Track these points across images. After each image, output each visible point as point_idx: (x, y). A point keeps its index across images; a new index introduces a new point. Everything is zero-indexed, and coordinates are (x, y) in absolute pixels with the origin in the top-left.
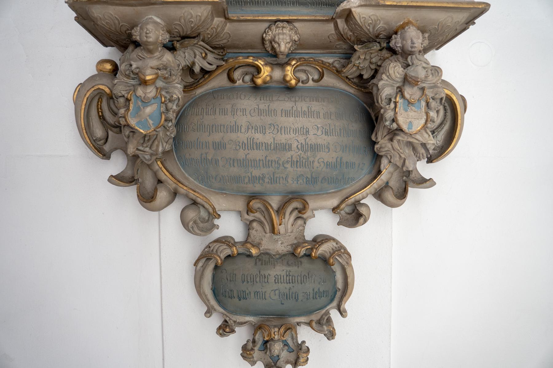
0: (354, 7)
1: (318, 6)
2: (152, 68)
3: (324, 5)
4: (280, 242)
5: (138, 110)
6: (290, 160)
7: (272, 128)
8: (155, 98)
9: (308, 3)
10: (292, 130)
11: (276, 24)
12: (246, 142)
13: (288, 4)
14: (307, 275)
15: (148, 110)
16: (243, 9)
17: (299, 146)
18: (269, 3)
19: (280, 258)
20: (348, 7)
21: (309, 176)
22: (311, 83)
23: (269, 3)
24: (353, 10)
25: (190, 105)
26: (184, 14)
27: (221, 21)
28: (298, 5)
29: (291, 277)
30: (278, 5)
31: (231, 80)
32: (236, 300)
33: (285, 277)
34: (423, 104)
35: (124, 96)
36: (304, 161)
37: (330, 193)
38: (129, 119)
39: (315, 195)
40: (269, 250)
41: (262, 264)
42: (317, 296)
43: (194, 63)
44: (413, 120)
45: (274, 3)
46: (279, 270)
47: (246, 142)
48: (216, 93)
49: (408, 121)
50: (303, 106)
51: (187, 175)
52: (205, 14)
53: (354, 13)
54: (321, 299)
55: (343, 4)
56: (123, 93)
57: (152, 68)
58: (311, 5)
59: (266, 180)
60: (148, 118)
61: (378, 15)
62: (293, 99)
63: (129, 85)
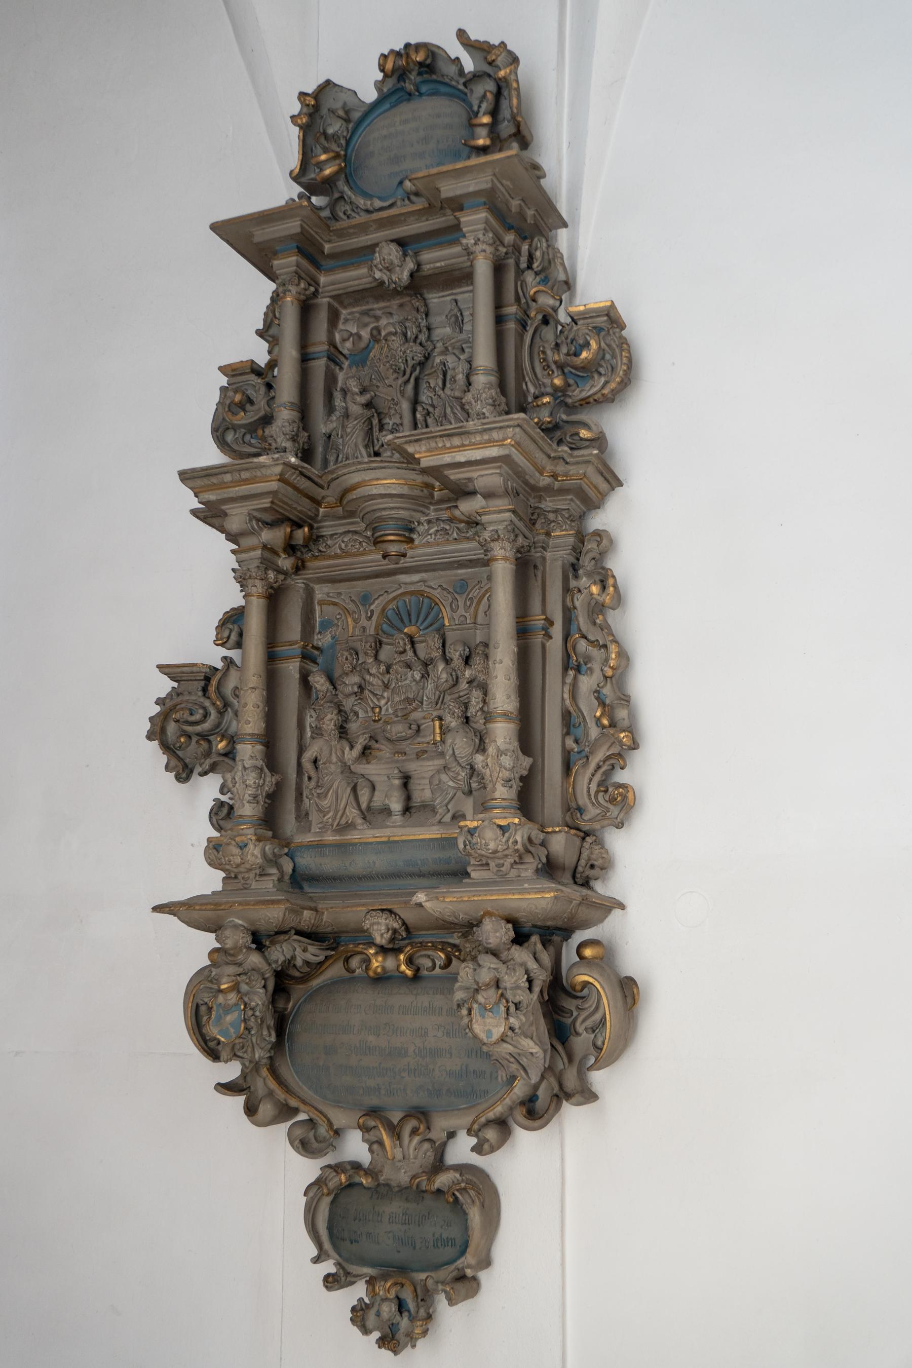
2: (228, 976)
4: (403, 1171)
5: (219, 1018)
6: (406, 1067)
7: (388, 1028)
8: (237, 1005)
10: (408, 1032)
12: (358, 1045)
14: (427, 1214)
15: (229, 1018)
17: (417, 1051)
19: (400, 1191)
21: (431, 1088)
22: (437, 970)
25: (305, 1001)
29: (407, 1217)
31: (349, 970)
32: (348, 1243)
33: (401, 1215)
34: (502, 1008)
35: (206, 1003)
36: (423, 1069)
37: (460, 1109)
38: (211, 1028)
39: (442, 1111)
40: (391, 1180)
41: (378, 1198)
42: (439, 1244)
43: (294, 957)
44: (491, 1028)
46: (395, 1207)
47: (358, 1045)
48: (336, 983)
49: (486, 1028)
50: (424, 1000)
51: (300, 1084)
52: (281, 915)
54: (446, 1248)
56: (206, 1000)
57: (228, 976)
59: (383, 1092)
60: (229, 1026)
62: (415, 992)
63: (213, 991)
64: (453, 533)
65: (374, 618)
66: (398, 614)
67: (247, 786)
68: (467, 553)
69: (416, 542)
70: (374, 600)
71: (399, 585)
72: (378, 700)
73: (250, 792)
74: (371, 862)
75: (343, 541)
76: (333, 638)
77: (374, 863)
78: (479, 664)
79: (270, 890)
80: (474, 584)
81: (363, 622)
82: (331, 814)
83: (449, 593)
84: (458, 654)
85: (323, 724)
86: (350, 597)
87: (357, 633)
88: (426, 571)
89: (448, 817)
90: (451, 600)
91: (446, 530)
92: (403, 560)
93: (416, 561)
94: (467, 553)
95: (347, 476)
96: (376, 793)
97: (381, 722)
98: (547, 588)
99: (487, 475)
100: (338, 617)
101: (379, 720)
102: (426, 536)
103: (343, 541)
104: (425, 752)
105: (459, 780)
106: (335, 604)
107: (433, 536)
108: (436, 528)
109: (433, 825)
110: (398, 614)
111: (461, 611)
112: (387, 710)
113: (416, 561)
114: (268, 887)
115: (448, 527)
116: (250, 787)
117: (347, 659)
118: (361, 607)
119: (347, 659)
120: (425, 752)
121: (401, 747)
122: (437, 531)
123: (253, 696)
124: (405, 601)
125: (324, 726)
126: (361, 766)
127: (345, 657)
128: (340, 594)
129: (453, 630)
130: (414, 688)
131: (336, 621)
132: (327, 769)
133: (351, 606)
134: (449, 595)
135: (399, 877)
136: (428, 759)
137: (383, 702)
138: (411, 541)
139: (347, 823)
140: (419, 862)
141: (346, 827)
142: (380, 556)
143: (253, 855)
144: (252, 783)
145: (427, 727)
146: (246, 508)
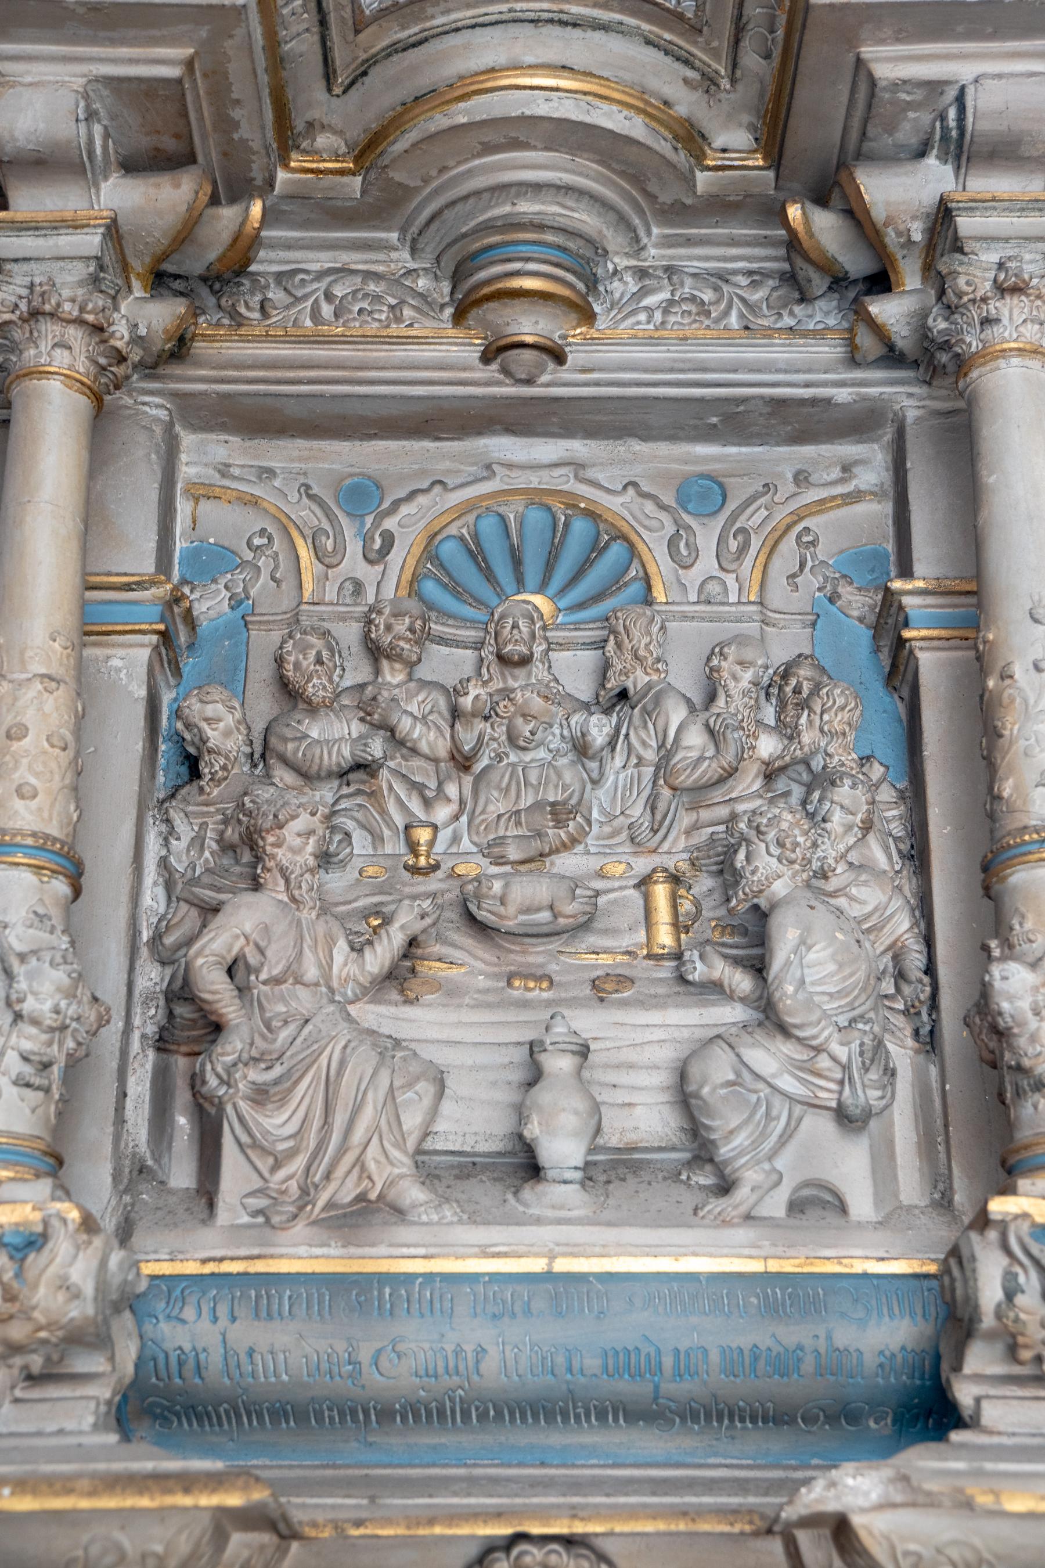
0: (863, 1510)
1: (715, 1424)
3: (742, 1420)
9: (668, 1414)
11: (515, 1552)
13: (577, 1417)
16: (371, 1439)
18: (492, 1413)
20: (832, 1506)
23: (492, 1413)
24: (857, 1520)
26: (86, 1549)
27: (262, 1548)
28: (621, 1421)
30: (530, 1420)
45: (512, 1414)
53: (863, 1535)
55: (809, 1491)
58: (683, 1419)
61: (977, 1542)
64: (726, 313)
65: (396, 557)
66: (477, 554)
67: (18, 1017)
68: (780, 377)
69: (601, 323)
70: (397, 504)
71: (488, 467)
72: (427, 803)
73: (27, 1045)
74: (469, 1348)
75: (329, 297)
76: (236, 603)
77: (481, 1351)
78: (842, 708)
79: (85, 1440)
80: (750, 491)
81: (353, 564)
82: (299, 1163)
83: (663, 507)
84: (748, 675)
85: (278, 845)
86: (308, 487)
87: (331, 595)
88: (591, 432)
89: (776, 1205)
90: (670, 529)
91: (703, 302)
92: (550, 372)
93: (597, 384)
94: (780, 377)
95: (466, 34)
96: (447, 1107)
97: (440, 874)
98: (133, 842)
99: (1012, 75)
100: (257, 541)
101: (436, 867)
102: (633, 312)
103: (329, 297)
104: (624, 981)
105: (819, 1075)
106: (253, 502)
107: (658, 316)
108: (665, 295)
109: (726, 1223)
110: (477, 554)
111: (707, 564)
112: (456, 839)
113: (597, 384)
114: (70, 1425)
115: (707, 296)
116: (35, 1022)
117: (319, 661)
118: (344, 520)
119: (319, 661)
120: (624, 981)
121: (531, 959)
122: (671, 302)
123: (50, 703)
124: (503, 519)
125: (280, 852)
126: (382, 1009)
127: (312, 655)
128: (271, 472)
129: (685, 617)
130: (568, 776)
131: (249, 555)
132: (282, 999)
133: (306, 514)
134: (664, 516)
135: (550, 1418)
136: (642, 1003)
137: (442, 813)
138: (588, 317)
139: (361, 1198)
140: (668, 1361)
141: (360, 1213)
142: (472, 354)
143: (64, 1284)
144: (48, 1005)
145: (615, 902)
146: (84, 68)
